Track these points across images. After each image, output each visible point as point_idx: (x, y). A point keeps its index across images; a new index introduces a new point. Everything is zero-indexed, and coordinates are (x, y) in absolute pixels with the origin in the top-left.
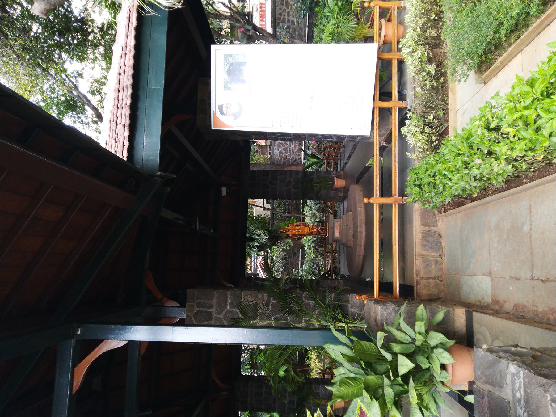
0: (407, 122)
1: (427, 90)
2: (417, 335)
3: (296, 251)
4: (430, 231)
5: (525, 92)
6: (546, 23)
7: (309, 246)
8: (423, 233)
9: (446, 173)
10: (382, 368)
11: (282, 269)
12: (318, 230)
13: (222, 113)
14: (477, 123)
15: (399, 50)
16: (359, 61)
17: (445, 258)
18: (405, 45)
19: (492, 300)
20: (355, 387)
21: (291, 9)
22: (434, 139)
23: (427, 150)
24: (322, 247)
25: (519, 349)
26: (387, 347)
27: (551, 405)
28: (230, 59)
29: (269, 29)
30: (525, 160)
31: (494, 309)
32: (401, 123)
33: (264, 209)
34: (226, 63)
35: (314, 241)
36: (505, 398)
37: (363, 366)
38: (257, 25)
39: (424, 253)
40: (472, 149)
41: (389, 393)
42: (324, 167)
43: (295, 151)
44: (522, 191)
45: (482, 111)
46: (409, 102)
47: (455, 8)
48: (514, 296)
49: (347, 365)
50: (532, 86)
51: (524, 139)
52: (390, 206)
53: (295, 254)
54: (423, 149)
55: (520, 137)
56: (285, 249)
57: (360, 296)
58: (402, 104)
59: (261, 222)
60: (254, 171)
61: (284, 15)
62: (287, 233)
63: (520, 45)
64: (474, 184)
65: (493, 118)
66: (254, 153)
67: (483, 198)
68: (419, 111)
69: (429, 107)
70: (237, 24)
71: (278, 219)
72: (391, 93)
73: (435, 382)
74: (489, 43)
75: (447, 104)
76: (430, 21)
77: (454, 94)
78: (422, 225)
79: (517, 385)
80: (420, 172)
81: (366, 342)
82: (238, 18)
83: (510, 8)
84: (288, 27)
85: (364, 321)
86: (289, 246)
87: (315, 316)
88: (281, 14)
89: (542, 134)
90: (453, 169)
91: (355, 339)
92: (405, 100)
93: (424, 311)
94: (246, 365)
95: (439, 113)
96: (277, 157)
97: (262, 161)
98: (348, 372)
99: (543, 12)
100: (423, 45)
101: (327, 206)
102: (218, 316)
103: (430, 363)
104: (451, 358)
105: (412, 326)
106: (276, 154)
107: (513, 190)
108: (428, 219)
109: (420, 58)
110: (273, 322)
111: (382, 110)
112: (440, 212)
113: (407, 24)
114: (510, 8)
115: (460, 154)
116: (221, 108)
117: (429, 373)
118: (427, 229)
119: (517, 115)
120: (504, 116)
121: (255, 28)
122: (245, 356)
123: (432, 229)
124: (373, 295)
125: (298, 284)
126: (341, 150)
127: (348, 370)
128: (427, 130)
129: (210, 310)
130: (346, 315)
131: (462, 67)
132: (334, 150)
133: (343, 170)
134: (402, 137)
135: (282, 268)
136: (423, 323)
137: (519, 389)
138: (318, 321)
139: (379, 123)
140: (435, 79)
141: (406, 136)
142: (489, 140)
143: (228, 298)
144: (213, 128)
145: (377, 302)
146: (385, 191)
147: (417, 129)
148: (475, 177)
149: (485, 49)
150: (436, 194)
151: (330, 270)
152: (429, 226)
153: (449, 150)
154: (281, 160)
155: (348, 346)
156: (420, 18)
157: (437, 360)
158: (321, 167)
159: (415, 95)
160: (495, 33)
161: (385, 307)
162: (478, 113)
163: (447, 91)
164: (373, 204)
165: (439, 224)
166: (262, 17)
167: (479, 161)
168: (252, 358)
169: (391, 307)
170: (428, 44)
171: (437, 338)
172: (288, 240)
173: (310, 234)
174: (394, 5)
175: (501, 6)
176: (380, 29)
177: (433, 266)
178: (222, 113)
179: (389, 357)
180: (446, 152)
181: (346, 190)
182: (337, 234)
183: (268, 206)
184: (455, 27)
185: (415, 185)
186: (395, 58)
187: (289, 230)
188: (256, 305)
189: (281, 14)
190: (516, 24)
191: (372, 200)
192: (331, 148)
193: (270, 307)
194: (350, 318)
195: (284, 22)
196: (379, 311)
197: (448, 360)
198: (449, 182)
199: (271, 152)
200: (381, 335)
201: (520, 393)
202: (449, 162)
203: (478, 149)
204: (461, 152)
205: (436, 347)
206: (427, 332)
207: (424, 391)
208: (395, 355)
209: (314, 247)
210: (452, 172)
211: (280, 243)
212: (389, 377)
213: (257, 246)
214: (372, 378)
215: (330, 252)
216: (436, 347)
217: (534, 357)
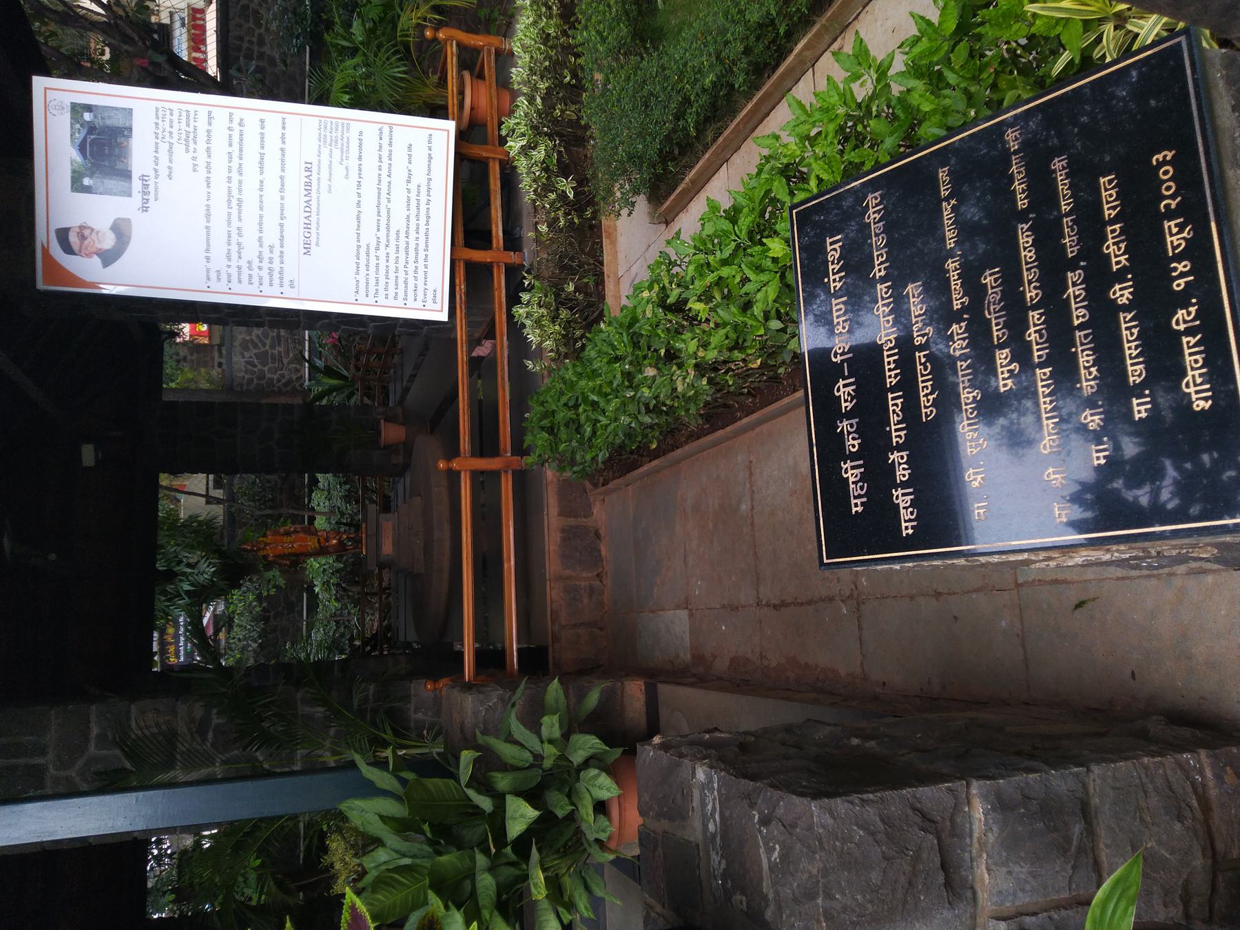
0: (525, 297)
1: (561, 230)
2: (546, 746)
3: (293, 599)
4: (576, 527)
5: (723, 230)
6: (764, 110)
7: (326, 584)
8: (563, 531)
9: (595, 398)
10: (472, 833)
11: (255, 645)
12: (340, 542)
13: (68, 249)
14: (646, 294)
15: (503, 141)
16: (416, 155)
17: (608, 582)
18: (514, 131)
19: (693, 656)
20: (409, 887)
21: (267, 30)
22: (578, 333)
23: (566, 357)
24: (357, 583)
25: (717, 734)
26: (481, 782)
27: (760, 832)
28: (87, 116)
29: (212, 69)
30: (730, 369)
31: (695, 673)
32: (513, 300)
33: (210, 500)
34: (78, 126)
35: (338, 571)
36: (692, 839)
37: (429, 835)
38: (185, 56)
39: (568, 572)
40: (639, 348)
41: (486, 883)
42: (356, 399)
43: (285, 361)
44: (737, 434)
45: (653, 271)
46: (527, 255)
47: (605, 62)
48: (731, 641)
49: (392, 840)
50: (734, 221)
51: (725, 324)
52: (495, 475)
53: (293, 607)
54: (558, 352)
55: (719, 321)
56: (265, 594)
57: (435, 681)
58: (513, 257)
59: (201, 534)
60: (172, 405)
61: (251, 42)
62: (261, 553)
63: (724, 148)
64: (647, 419)
65: (671, 283)
66: (178, 361)
67: (670, 451)
68: (546, 274)
69: (566, 270)
70: (125, 47)
71: (245, 524)
72: (490, 232)
73: (586, 845)
74: (668, 138)
75: (602, 263)
76: (561, 85)
77: (614, 243)
78: (560, 514)
79: (710, 807)
80: (550, 400)
81: (436, 780)
82: (129, 32)
83: (700, 71)
84: (259, 70)
85: (440, 739)
86: (275, 586)
87: (328, 744)
88: (241, 39)
89: (753, 315)
90: (607, 390)
91: (409, 776)
92: (520, 250)
93: (561, 692)
94: (164, 893)
95: (586, 280)
96: (241, 374)
97: (204, 385)
98: (395, 855)
99: (758, 89)
100: (550, 136)
101: (365, 489)
102: (63, 773)
103: (573, 804)
104: (615, 786)
105: (535, 727)
106: (236, 367)
107: (720, 433)
108: (573, 504)
109: (544, 162)
110: (218, 770)
111: (471, 267)
112: (595, 485)
113: (516, 87)
114: (700, 71)
115: (617, 359)
116: (63, 234)
117: (573, 826)
118: (571, 521)
119: (711, 278)
120: (688, 278)
121: (174, 60)
122: (157, 870)
123: (583, 521)
124: (463, 677)
125: (296, 673)
126: (396, 359)
127: (397, 852)
128: (564, 314)
129: (39, 761)
130: (402, 729)
131: (622, 187)
132: (379, 357)
133: (401, 402)
134: (515, 329)
135: (255, 641)
136: (555, 718)
137: (713, 814)
138: (335, 753)
139: (468, 294)
140: (575, 210)
141: (523, 326)
142: (668, 329)
143: (92, 725)
144: (41, 285)
145: (468, 687)
146: (486, 444)
147: (543, 311)
148: (647, 406)
149: (661, 150)
150: (581, 443)
151: (374, 636)
152: (576, 516)
153: (599, 352)
154: (250, 381)
155: (398, 798)
156: (542, 78)
157: (587, 796)
158: (349, 397)
159: (537, 241)
160: (677, 118)
161: (481, 697)
162: (645, 276)
163: (600, 237)
164: (459, 473)
165: (595, 511)
166: (198, 41)
167: (650, 372)
168: (179, 879)
169: (495, 695)
170: (561, 136)
171: (587, 744)
172: (271, 573)
173: (322, 551)
174: (490, 44)
175: (685, 65)
176: (461, 93)
177: (586, 601)
178: (68, 249)
179: (485, 803)
180: (593, 354)
181: (407, 447)
182: (387, 548)
183: (219, 494)
184: (607, 102)
185: (543, 428)
186: (494, 159)
187: (266, 544)
188: (171, 737)
189: (241, 39)
190: (714, 106)
191: (455, 465)
192: (370, 353)
193: (210, 735)
194: (413, 735)
195: (249, 57)
196: (469, 707)
197: (608, 790)
198: (601, 418)
199: (223, 361)
200: (467, 756)
201: (715, 821)
202: (600, 375)
203: (649, 349)
204: (618, 353)
205: (586, 764)
206: (566, 736)
207: (562, 866)
208: (499, 799)
209: (338, 585)
210: (606, 395)
211: (250, 580)
212: (486, 851)
213: (188, 592)
214: (449, 859)
215: (375, 594)
216: (586, 764)
217: (743, 747)
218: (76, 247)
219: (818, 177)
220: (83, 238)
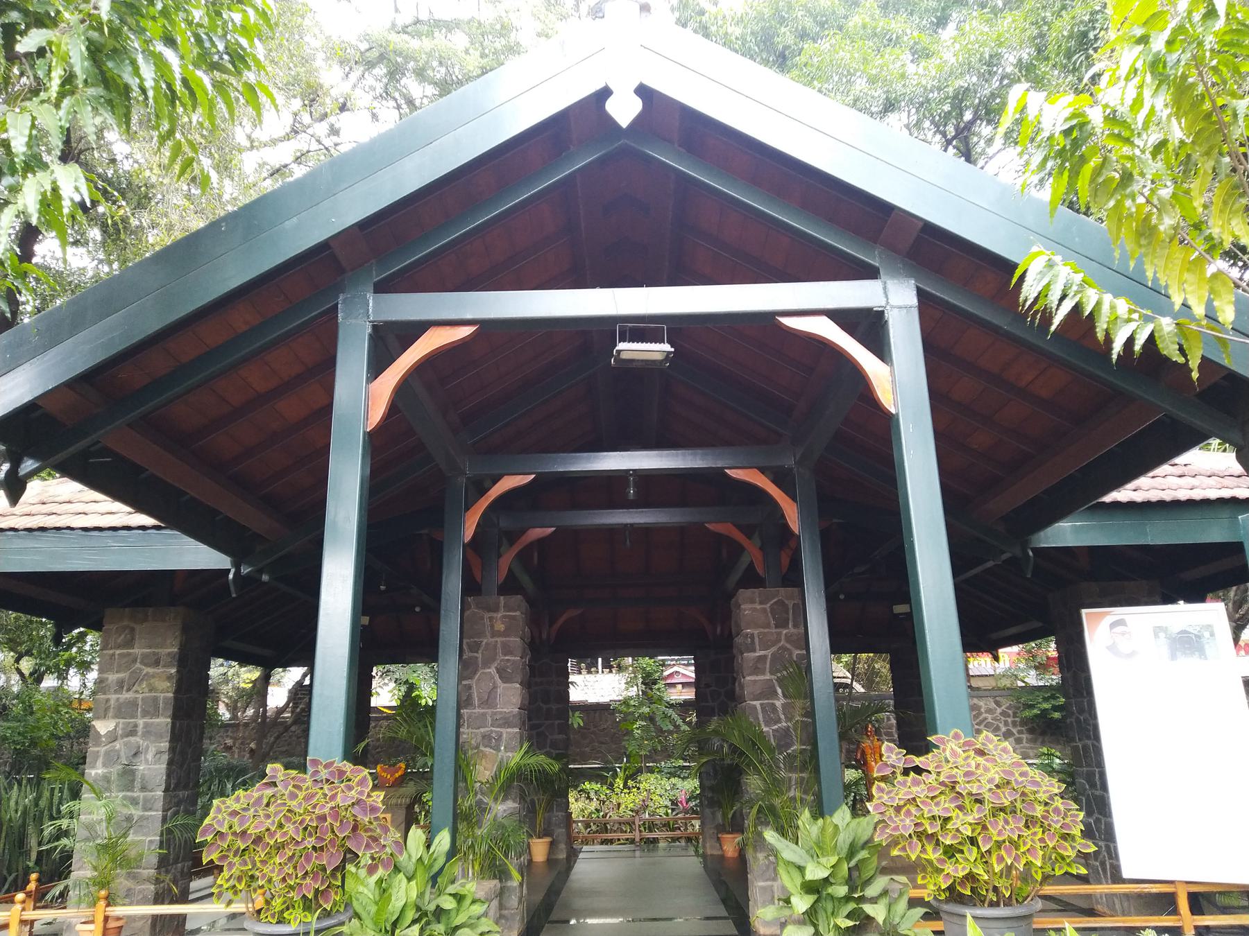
28: (1207, 634)
139: (1150, 894)
178: (1113, 625)
218: (1115, 630)
219: (66, 887)
220: (1123, 634)
